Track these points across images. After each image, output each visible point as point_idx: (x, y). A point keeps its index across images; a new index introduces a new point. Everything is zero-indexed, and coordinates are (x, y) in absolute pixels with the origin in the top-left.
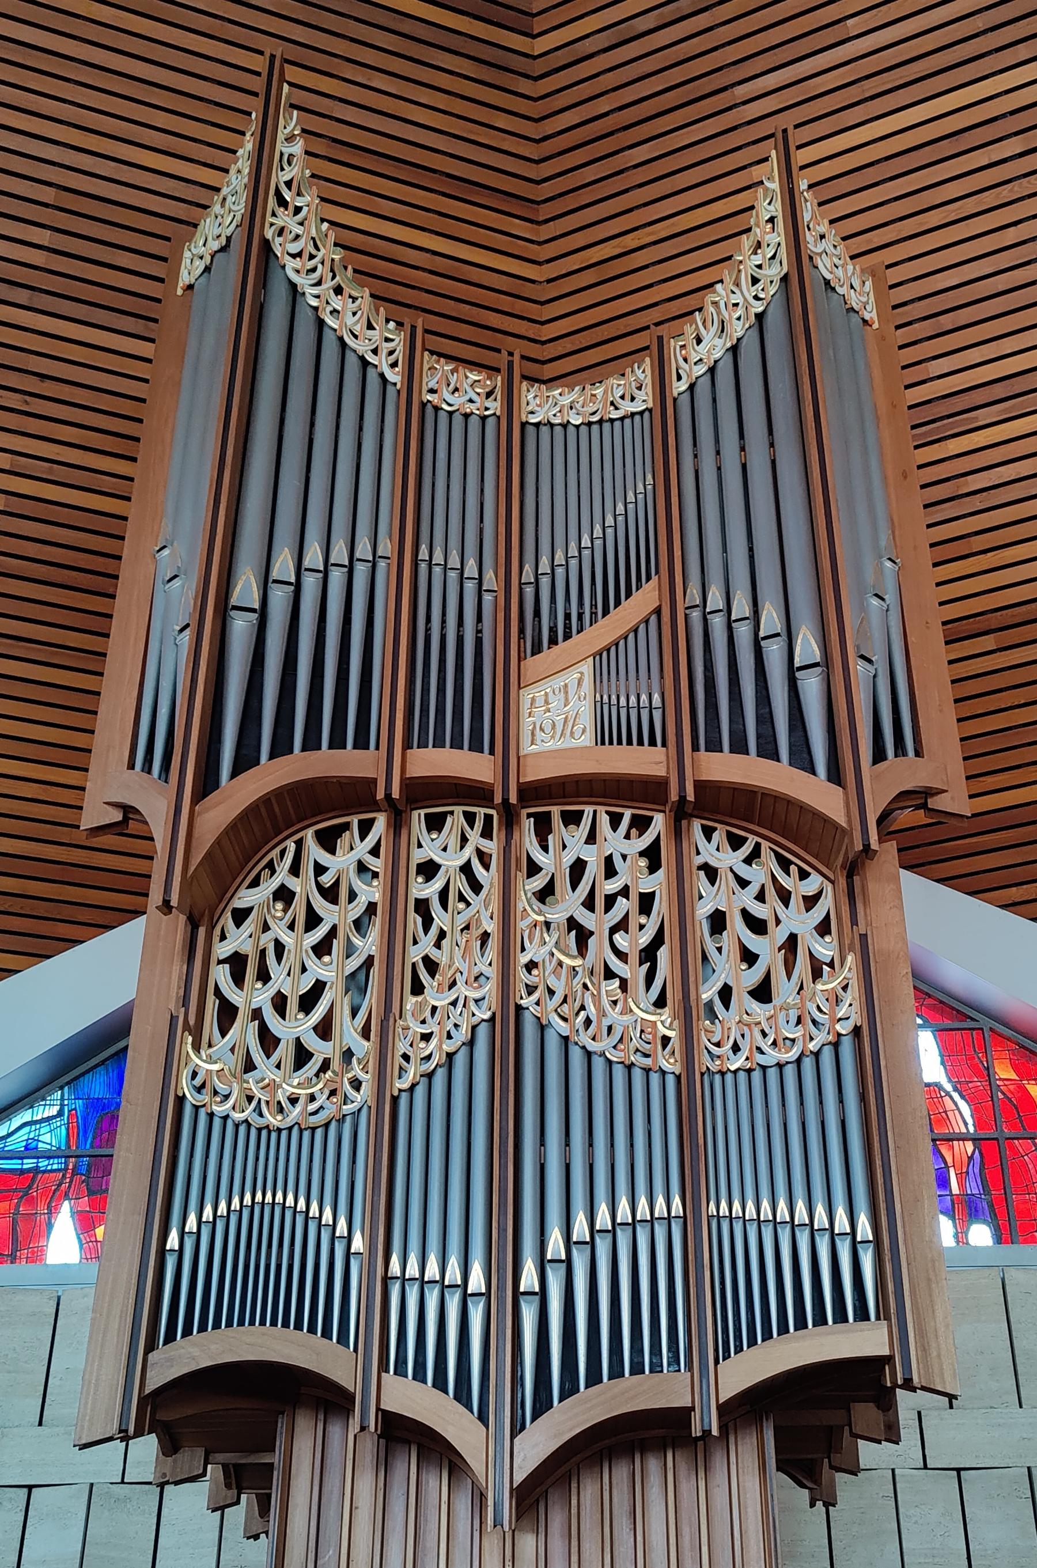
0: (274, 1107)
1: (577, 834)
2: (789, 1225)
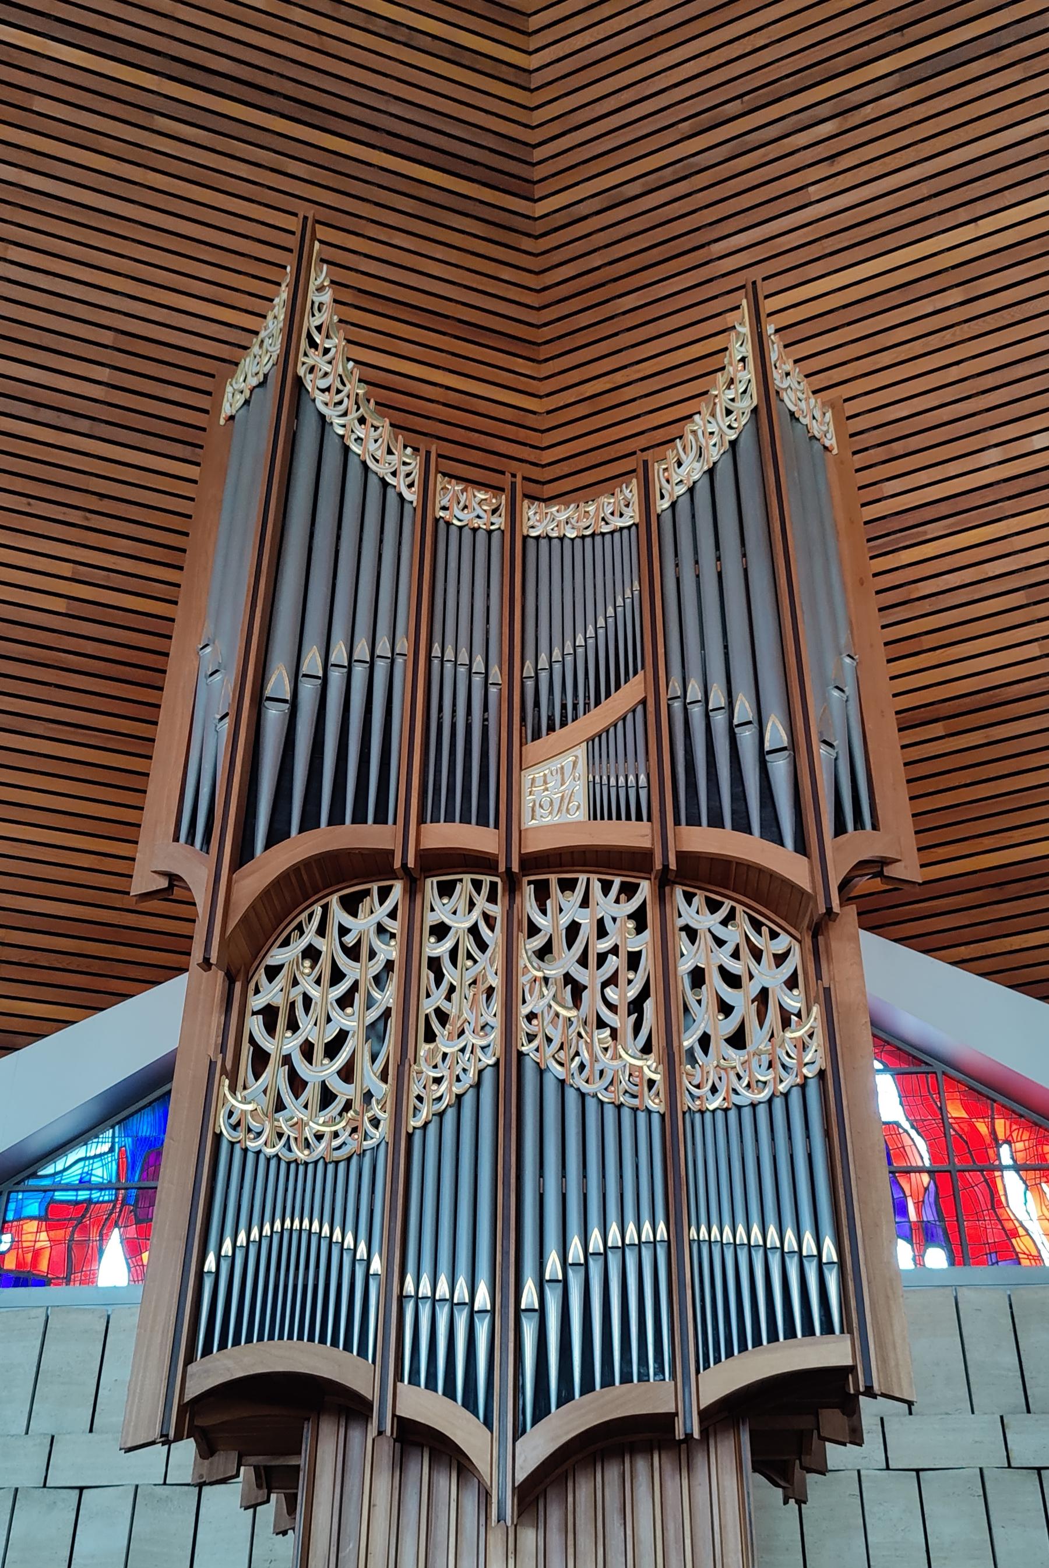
0: (302, 1143)
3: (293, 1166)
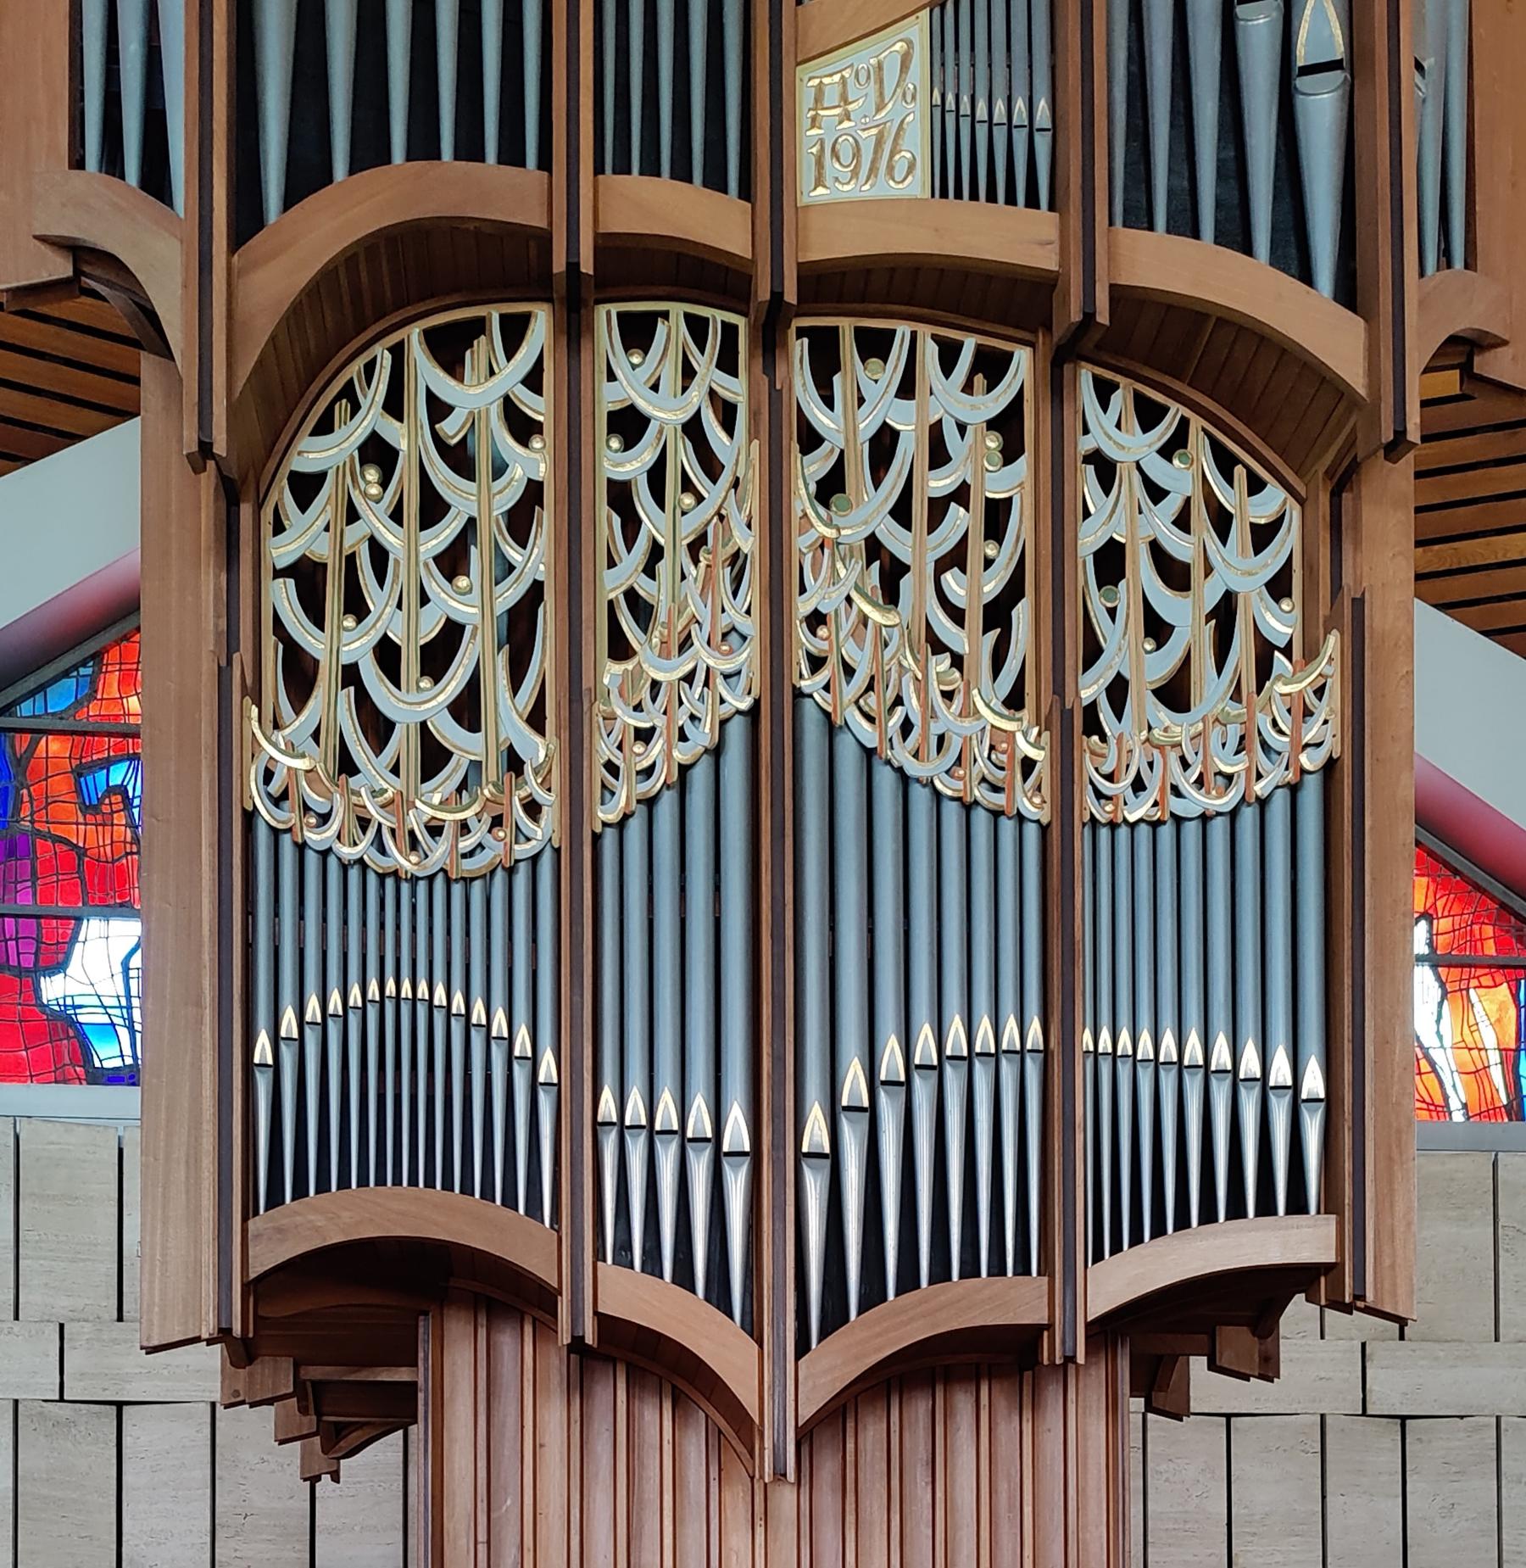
0: (405, 841)
1: (884, 378)
2: (1202, 1071)
3: (390, 882)
